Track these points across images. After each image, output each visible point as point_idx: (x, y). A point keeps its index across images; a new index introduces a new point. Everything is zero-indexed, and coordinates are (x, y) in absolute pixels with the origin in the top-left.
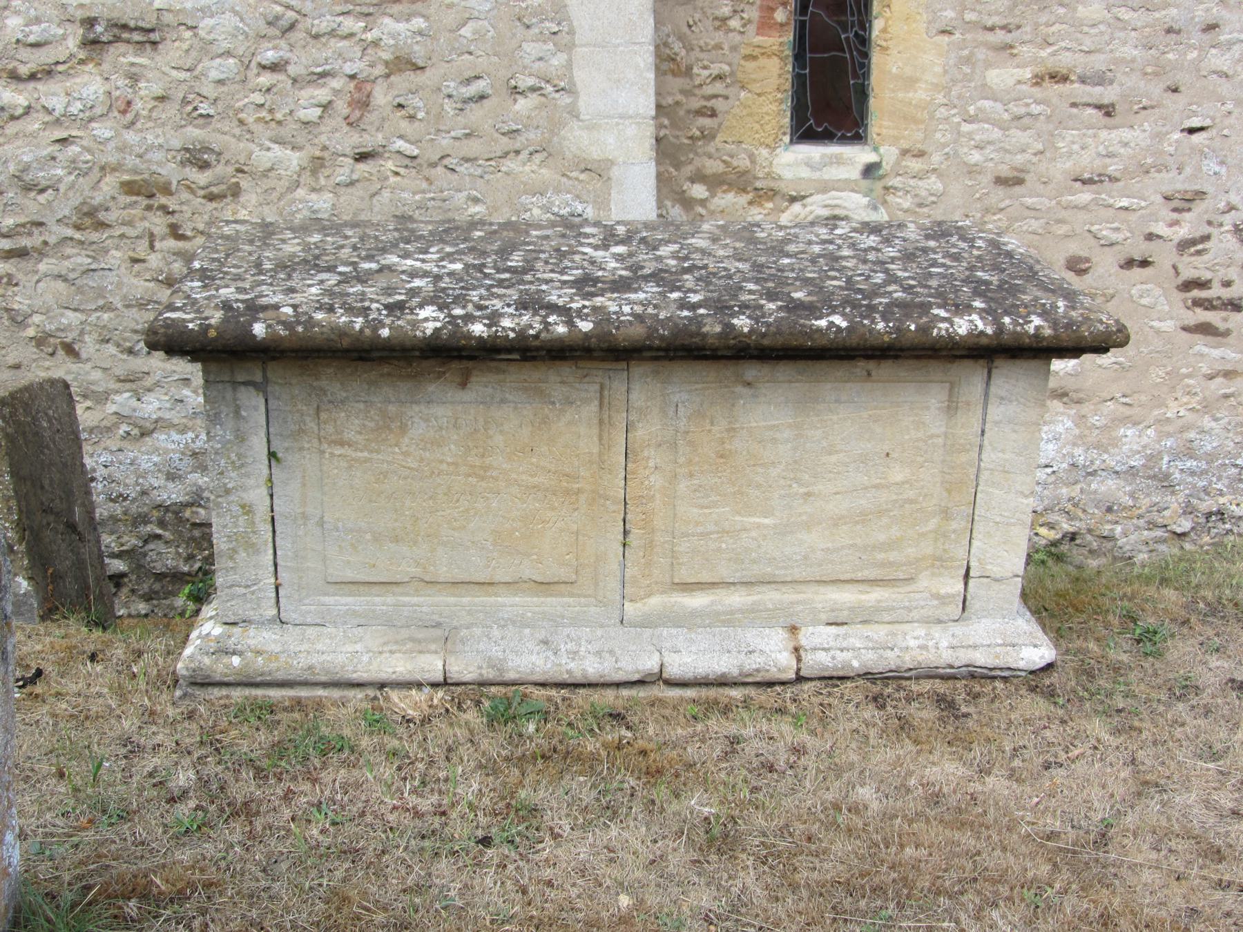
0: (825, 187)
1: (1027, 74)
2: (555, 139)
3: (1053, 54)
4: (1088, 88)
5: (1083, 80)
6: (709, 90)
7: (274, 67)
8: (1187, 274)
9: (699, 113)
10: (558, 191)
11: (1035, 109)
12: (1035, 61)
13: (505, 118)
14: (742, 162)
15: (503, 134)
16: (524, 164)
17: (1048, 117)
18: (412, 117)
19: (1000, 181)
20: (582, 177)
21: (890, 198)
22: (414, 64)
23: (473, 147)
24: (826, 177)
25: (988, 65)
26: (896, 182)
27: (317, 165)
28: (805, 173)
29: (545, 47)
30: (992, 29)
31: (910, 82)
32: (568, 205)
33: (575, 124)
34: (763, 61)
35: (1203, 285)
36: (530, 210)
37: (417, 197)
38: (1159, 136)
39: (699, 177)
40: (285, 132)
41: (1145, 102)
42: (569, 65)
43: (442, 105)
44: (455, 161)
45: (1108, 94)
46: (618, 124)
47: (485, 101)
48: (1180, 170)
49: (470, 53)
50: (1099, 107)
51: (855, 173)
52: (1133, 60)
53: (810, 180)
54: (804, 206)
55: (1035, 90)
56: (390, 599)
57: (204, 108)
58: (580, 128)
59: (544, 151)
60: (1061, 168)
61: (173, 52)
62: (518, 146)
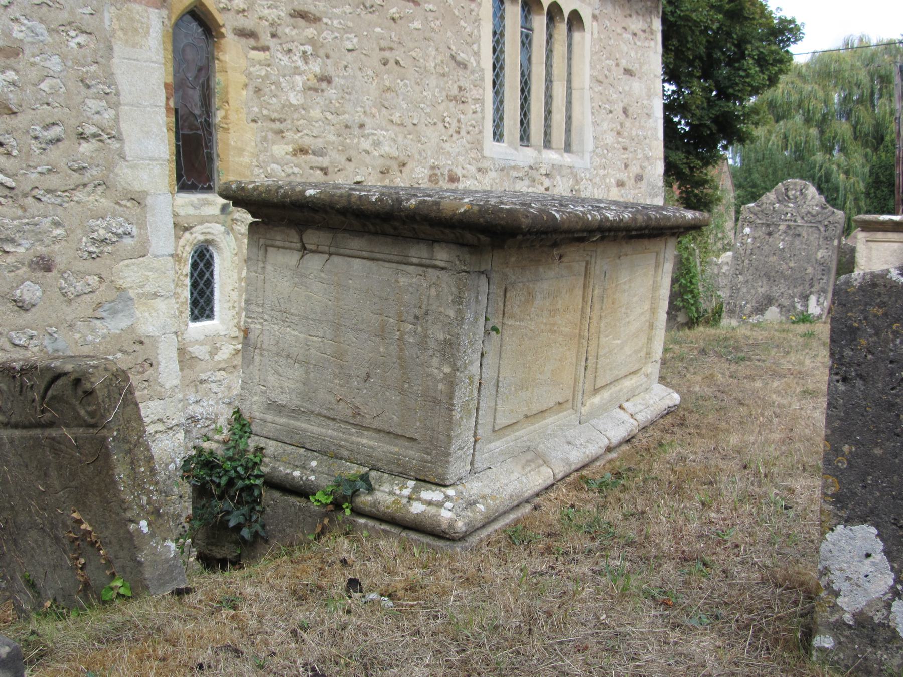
0: (203, 220)
1: (290, 149)
2: (112, 175)
3: (301, 137)
4: (316, 158)
5: (314, 154)
10: (114, 216)
11: (296, 170)
12: (294, 142)
13: (75, 158)
15: (74, 170)
16: (89, 195)
17: (302, 175)
18: (9, 154)
20: (129, 204)
21: (235, 226)
22: (10, 109)
23: (54, 181)
24: (203, 213)
25: (274, 143)
28: (191, 211)
29: (101, 104)
30: (273, 121)
31: (241, 151)
32: (122, 226)
33: (123, 163)
36: (97, 231)
37: (16, 222)
41: (340, 167)
42: (117, 119)
43: (30, 145)
44: (41, 192)
46: (149, 165)
47: (59, 144)
49: (48, 104)
50: (321, 169)
52: (333, 143)
53: (195, 216)
54: (191, 233)
55: (294, 159)
56: (513, 437)
58: (128, 167)
59: (103, 184)
62: (86, 180)
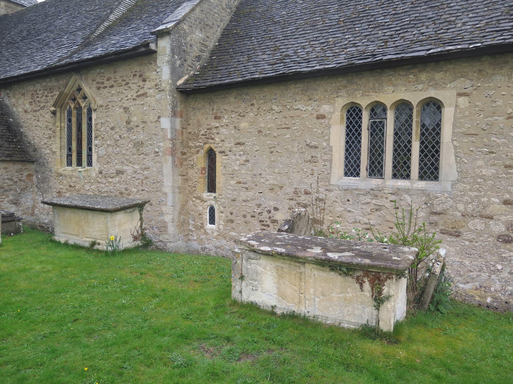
0: (210, 200)
1: (235, 182)
6: (195, 183)
7: (134, 177)
8: (260, 219)
9: (194, 187)
11: (237, 188)
14: (199, 195)
19: (232, 200)
25: (230, 181)
26: (218, 199)
27: (138, 191)
28: (207, 197)
30: (230, 174)
34: (201, 179)
35: (263, 221)
38: (255, 194)
39: (194, 197)
40: (135, 186)
45: (246, 186)
48: (258, 200)
51: (212, 198)
57: (128, 183)
60: (241, 199)
61: (125, 175)
